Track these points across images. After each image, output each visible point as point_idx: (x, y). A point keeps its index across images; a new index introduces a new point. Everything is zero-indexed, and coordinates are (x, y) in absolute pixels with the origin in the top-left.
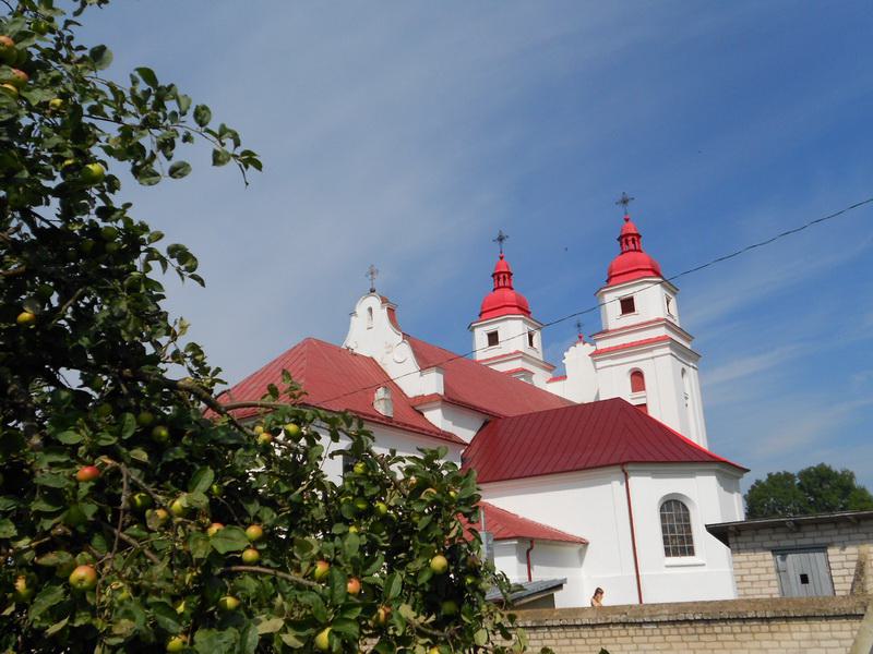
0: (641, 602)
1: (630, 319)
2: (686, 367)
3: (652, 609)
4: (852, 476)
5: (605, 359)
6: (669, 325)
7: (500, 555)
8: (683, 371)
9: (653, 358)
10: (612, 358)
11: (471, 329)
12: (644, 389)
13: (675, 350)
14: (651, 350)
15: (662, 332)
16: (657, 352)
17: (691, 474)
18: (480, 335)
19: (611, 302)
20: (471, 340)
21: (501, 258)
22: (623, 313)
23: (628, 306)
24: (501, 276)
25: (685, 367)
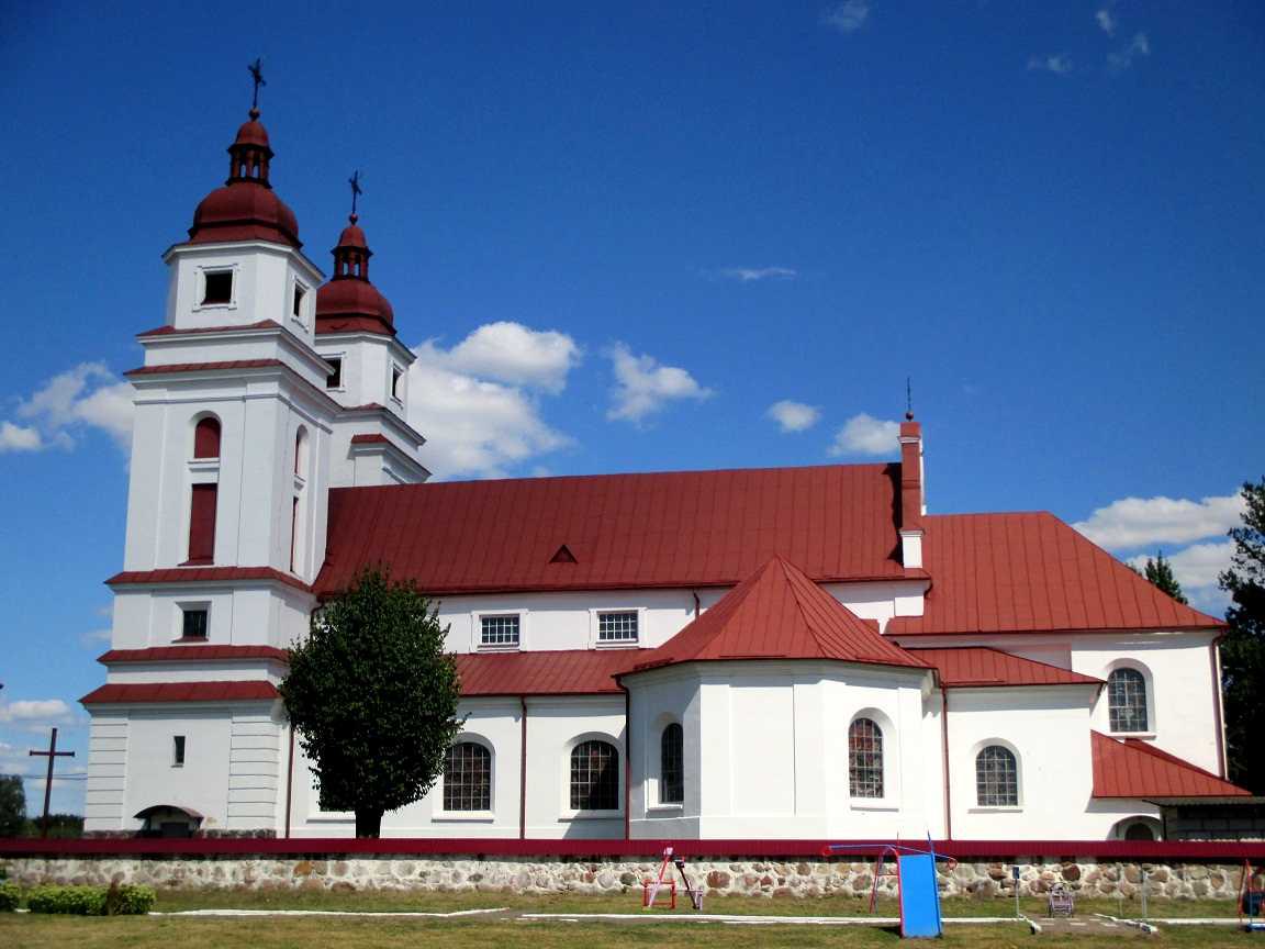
0: (45, 754)
1: (217, 316)
2: (309, 426)
3: (777, 911)
4: (275, 832)
5: (159, 386)
6: (286, 339)
7: (445, 613)
8: (301, 434)
9: (244, 399)
10: (171, 386)
11: (171, 259)
12: (217, 454)
13: (293, 390)
14: (243, 382)
15: (269, 350)
16: (253, 389)
17: (893, 685)
18: (191, 275)
19: (191, 275)
20: (168, 282)
21: (254, 116)
22: (207, 301)
23: (219, 288)
24: (252, 153)
25: (306, 423)
